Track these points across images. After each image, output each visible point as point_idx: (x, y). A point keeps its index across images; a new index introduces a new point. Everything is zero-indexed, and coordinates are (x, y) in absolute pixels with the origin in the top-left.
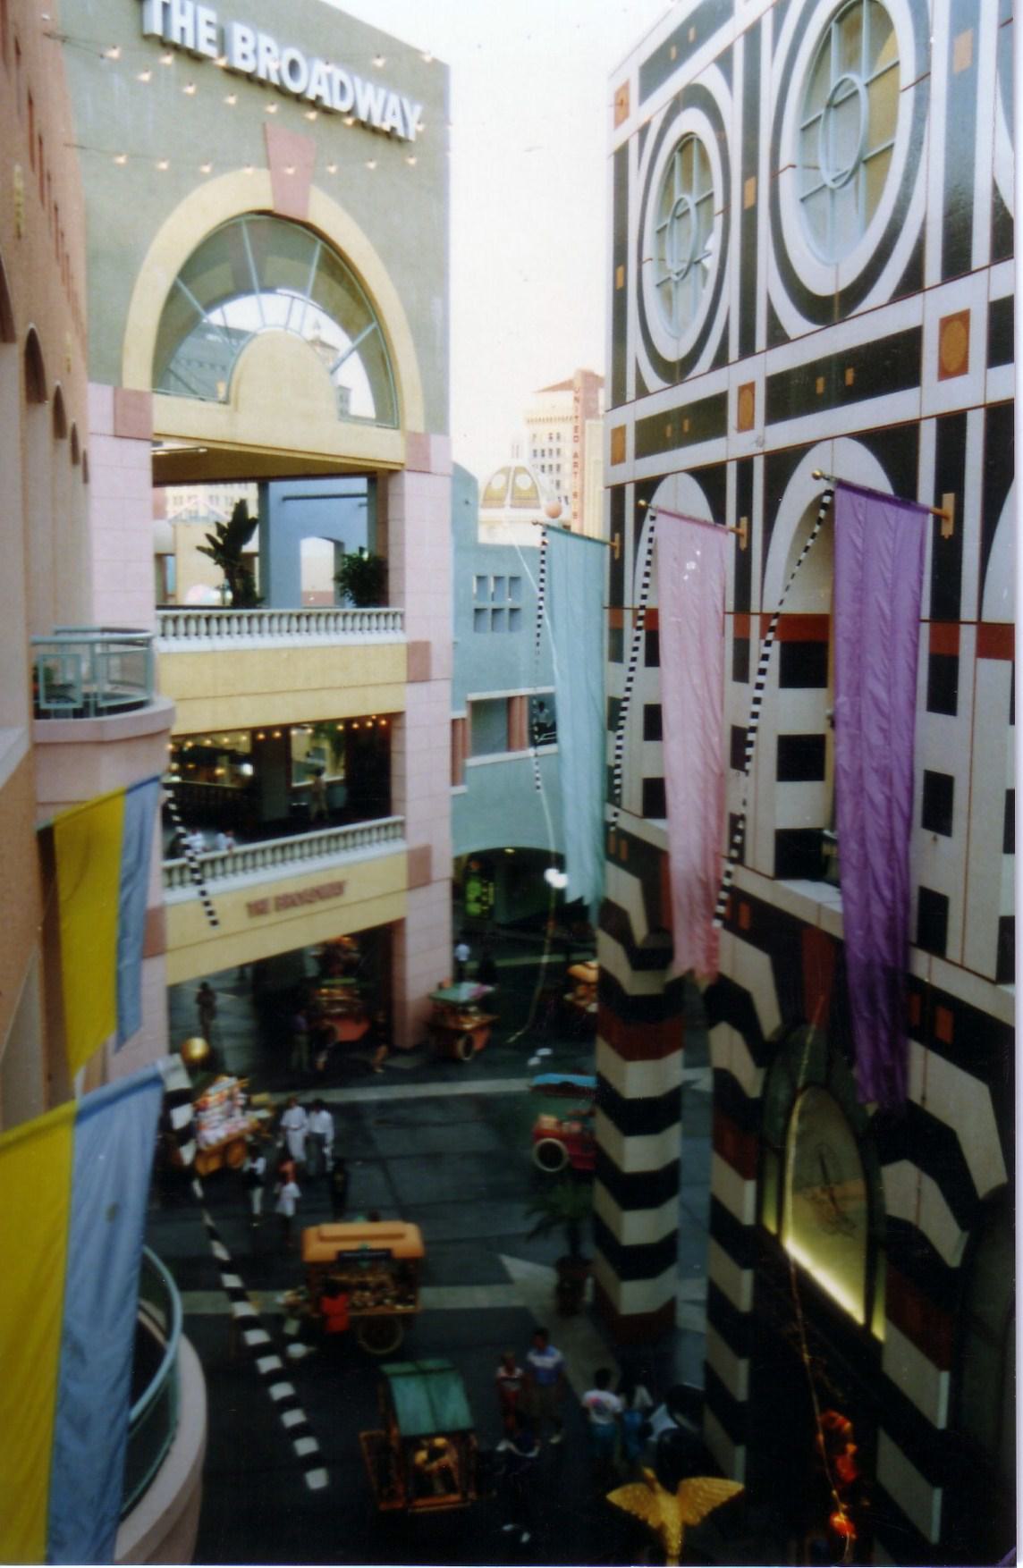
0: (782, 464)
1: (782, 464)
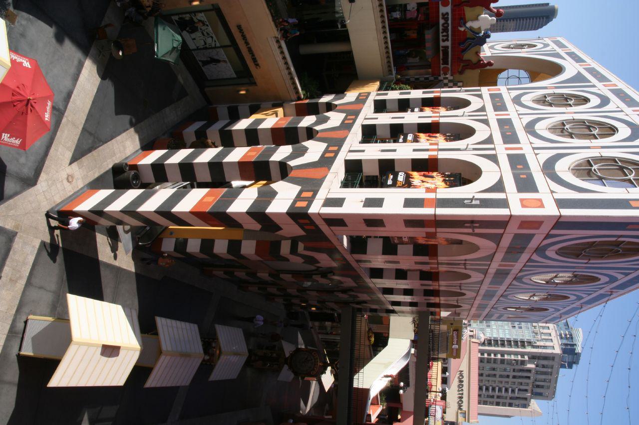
0: (494, 158)
1: (494, 158)
